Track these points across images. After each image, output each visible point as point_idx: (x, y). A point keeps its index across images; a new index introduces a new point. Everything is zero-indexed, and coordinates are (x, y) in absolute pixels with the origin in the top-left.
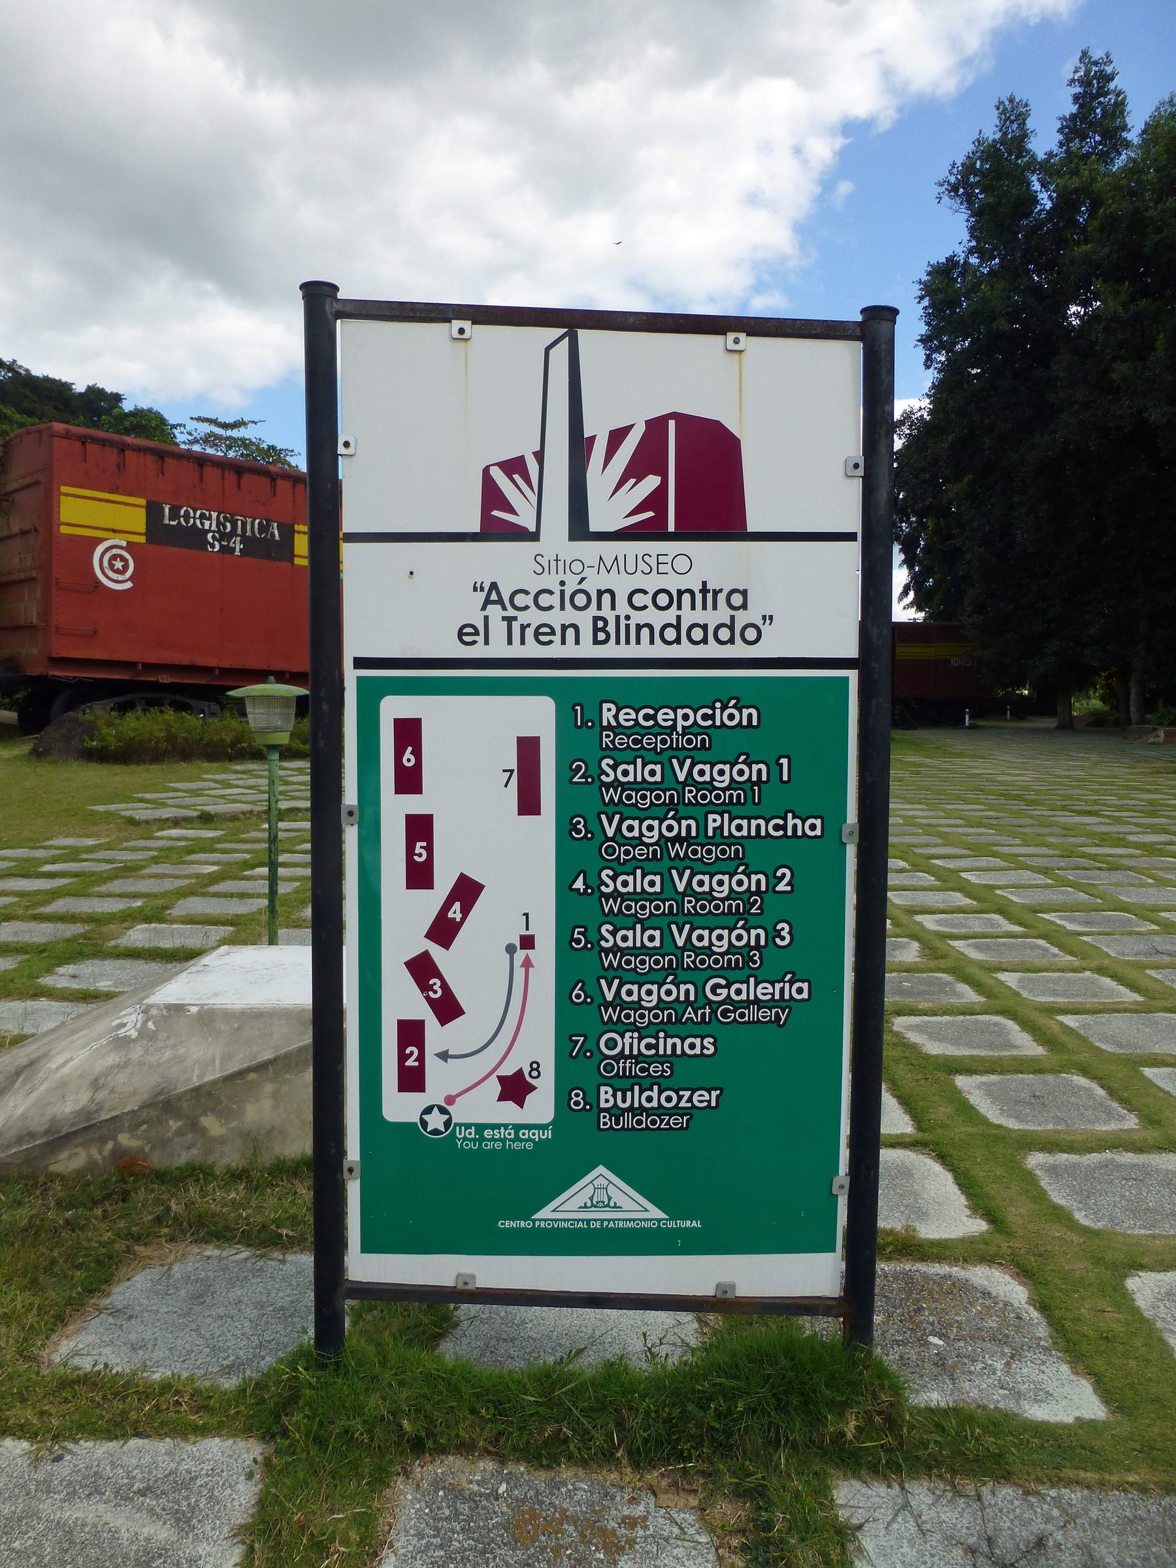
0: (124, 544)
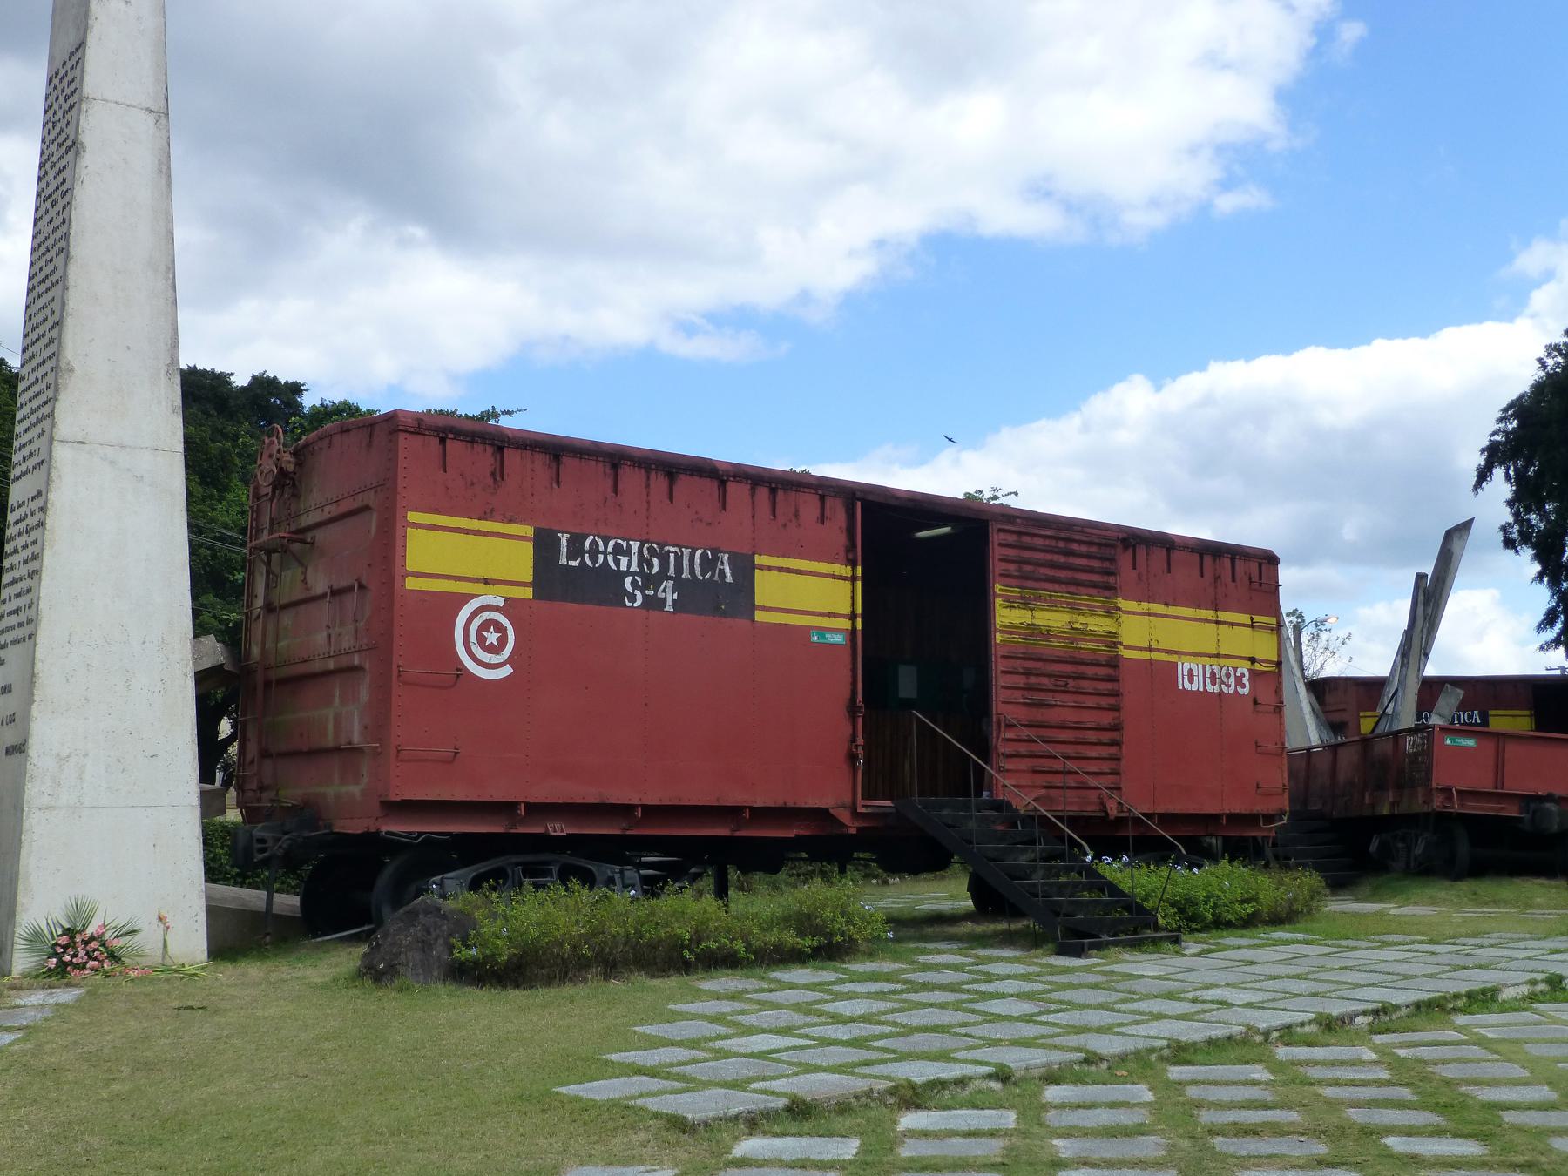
0: (500, 602)
